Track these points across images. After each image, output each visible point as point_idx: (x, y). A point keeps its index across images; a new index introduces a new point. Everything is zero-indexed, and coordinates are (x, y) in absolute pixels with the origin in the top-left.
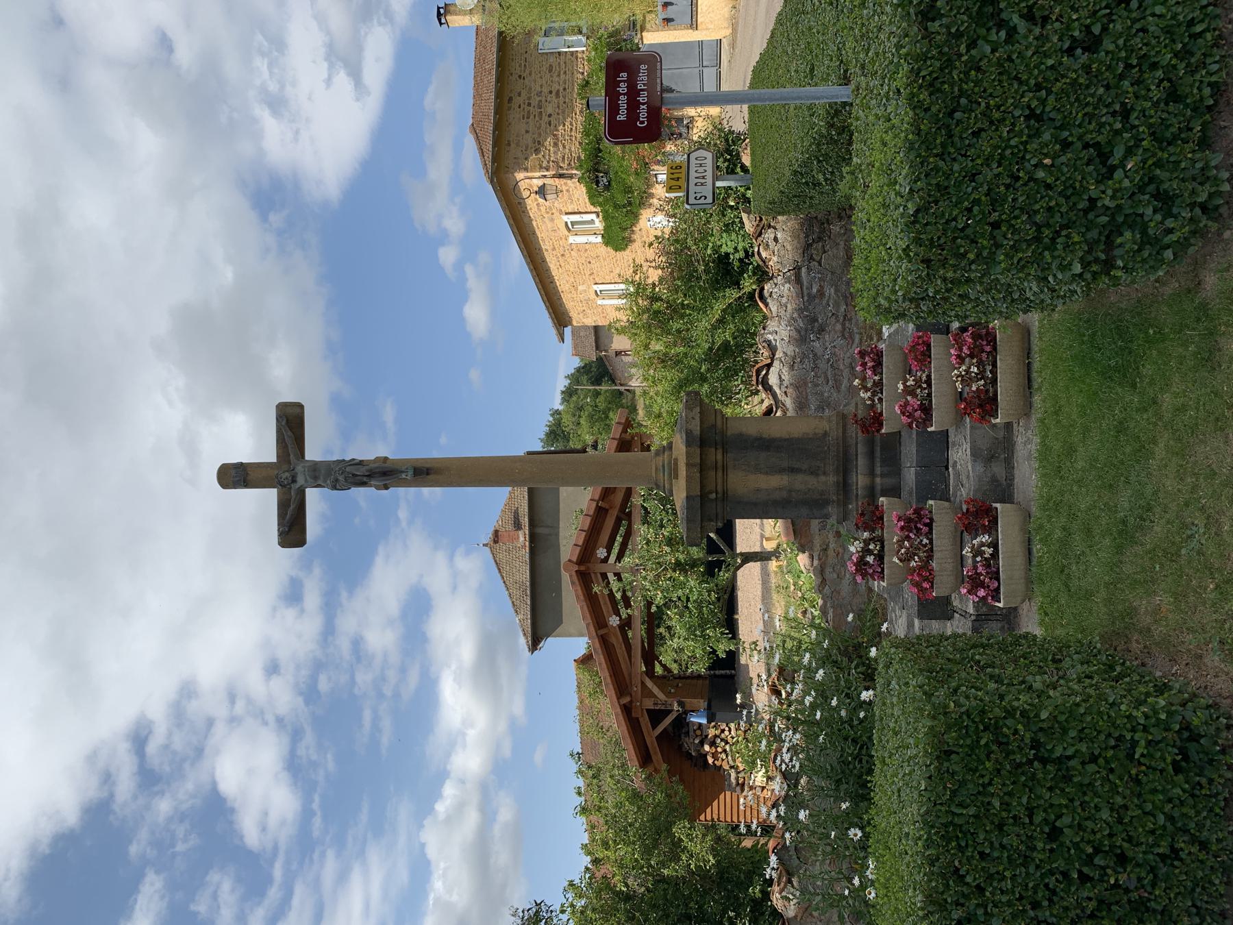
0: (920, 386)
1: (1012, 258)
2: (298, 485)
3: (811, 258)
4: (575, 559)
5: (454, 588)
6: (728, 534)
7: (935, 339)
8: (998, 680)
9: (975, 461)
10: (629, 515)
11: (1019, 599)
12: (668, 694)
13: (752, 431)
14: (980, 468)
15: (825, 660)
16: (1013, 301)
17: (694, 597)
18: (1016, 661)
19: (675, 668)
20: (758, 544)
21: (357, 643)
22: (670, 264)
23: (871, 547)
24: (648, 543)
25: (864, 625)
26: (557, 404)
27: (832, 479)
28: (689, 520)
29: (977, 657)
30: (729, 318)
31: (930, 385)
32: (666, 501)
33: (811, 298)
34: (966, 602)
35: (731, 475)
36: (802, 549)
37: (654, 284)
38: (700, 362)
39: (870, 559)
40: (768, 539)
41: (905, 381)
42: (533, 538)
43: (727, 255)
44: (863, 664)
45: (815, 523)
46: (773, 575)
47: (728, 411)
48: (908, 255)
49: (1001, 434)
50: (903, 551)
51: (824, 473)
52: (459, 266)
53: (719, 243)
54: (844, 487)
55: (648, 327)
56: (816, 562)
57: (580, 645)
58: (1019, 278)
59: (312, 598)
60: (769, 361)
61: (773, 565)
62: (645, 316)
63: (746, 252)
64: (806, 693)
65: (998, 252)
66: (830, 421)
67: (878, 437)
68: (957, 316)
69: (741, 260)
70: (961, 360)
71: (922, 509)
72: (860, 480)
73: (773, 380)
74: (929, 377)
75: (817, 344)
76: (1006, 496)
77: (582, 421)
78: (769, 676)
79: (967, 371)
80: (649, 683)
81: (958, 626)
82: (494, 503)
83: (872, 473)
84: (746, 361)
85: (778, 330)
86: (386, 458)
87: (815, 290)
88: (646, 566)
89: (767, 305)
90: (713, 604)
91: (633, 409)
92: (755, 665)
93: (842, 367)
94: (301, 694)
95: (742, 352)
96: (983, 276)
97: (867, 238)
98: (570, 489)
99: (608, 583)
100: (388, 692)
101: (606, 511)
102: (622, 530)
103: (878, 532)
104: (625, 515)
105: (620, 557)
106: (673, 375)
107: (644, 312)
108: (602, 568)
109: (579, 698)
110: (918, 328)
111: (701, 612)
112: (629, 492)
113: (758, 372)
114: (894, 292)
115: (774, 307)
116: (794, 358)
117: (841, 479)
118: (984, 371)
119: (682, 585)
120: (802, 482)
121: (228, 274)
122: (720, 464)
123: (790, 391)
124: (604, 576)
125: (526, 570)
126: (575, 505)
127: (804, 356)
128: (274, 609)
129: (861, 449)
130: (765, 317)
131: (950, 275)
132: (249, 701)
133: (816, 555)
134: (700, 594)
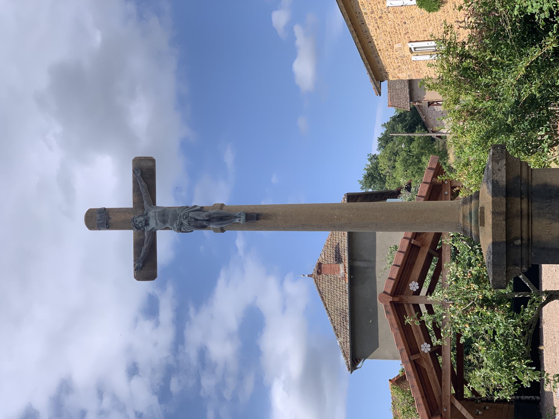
2: (149, 228)
4: (389, 291)
5: (284, 309)
6: (535, 276)
10: (440, 252)
21: (203, 353)
22: (479, 24)
24: (457, 280)
26: (375, 150)
28: (495, 265)
30: (535, 74)
32: (474, 242)
38: (505, 115)
42: (352, 270)
43: (533, 15)
47: (532, 161)
52: (289, 27)
55: (458, 85)
57: (395, 367)
59: (166, 313)
62: (455, 73)
69: (545, 20)
77: (397, 165)
80: (458, 405)
82: (317, 244)
86: (222, 205)
88: (455, 299)
90: (519, 338)
91: (444, 154)
94: (155, 393)
95: (548, 105)
98: (381, 233)
99: (420, 314)
100: (227, 395)
101: (419, 248)
102: (433, 265)
104: (436, 251)
105: (430, 291)
106: (483, 126)
107: (454, 69)
111: (507, 345)
112: (438, 236)
119: (490, 320)
121: (98, 38)
122: (525, 212)
124: (417, 307)
125: (347, 298)
126: (388, 249)
128: (136, 320)
132: (115, 398)
134: (506, 328)
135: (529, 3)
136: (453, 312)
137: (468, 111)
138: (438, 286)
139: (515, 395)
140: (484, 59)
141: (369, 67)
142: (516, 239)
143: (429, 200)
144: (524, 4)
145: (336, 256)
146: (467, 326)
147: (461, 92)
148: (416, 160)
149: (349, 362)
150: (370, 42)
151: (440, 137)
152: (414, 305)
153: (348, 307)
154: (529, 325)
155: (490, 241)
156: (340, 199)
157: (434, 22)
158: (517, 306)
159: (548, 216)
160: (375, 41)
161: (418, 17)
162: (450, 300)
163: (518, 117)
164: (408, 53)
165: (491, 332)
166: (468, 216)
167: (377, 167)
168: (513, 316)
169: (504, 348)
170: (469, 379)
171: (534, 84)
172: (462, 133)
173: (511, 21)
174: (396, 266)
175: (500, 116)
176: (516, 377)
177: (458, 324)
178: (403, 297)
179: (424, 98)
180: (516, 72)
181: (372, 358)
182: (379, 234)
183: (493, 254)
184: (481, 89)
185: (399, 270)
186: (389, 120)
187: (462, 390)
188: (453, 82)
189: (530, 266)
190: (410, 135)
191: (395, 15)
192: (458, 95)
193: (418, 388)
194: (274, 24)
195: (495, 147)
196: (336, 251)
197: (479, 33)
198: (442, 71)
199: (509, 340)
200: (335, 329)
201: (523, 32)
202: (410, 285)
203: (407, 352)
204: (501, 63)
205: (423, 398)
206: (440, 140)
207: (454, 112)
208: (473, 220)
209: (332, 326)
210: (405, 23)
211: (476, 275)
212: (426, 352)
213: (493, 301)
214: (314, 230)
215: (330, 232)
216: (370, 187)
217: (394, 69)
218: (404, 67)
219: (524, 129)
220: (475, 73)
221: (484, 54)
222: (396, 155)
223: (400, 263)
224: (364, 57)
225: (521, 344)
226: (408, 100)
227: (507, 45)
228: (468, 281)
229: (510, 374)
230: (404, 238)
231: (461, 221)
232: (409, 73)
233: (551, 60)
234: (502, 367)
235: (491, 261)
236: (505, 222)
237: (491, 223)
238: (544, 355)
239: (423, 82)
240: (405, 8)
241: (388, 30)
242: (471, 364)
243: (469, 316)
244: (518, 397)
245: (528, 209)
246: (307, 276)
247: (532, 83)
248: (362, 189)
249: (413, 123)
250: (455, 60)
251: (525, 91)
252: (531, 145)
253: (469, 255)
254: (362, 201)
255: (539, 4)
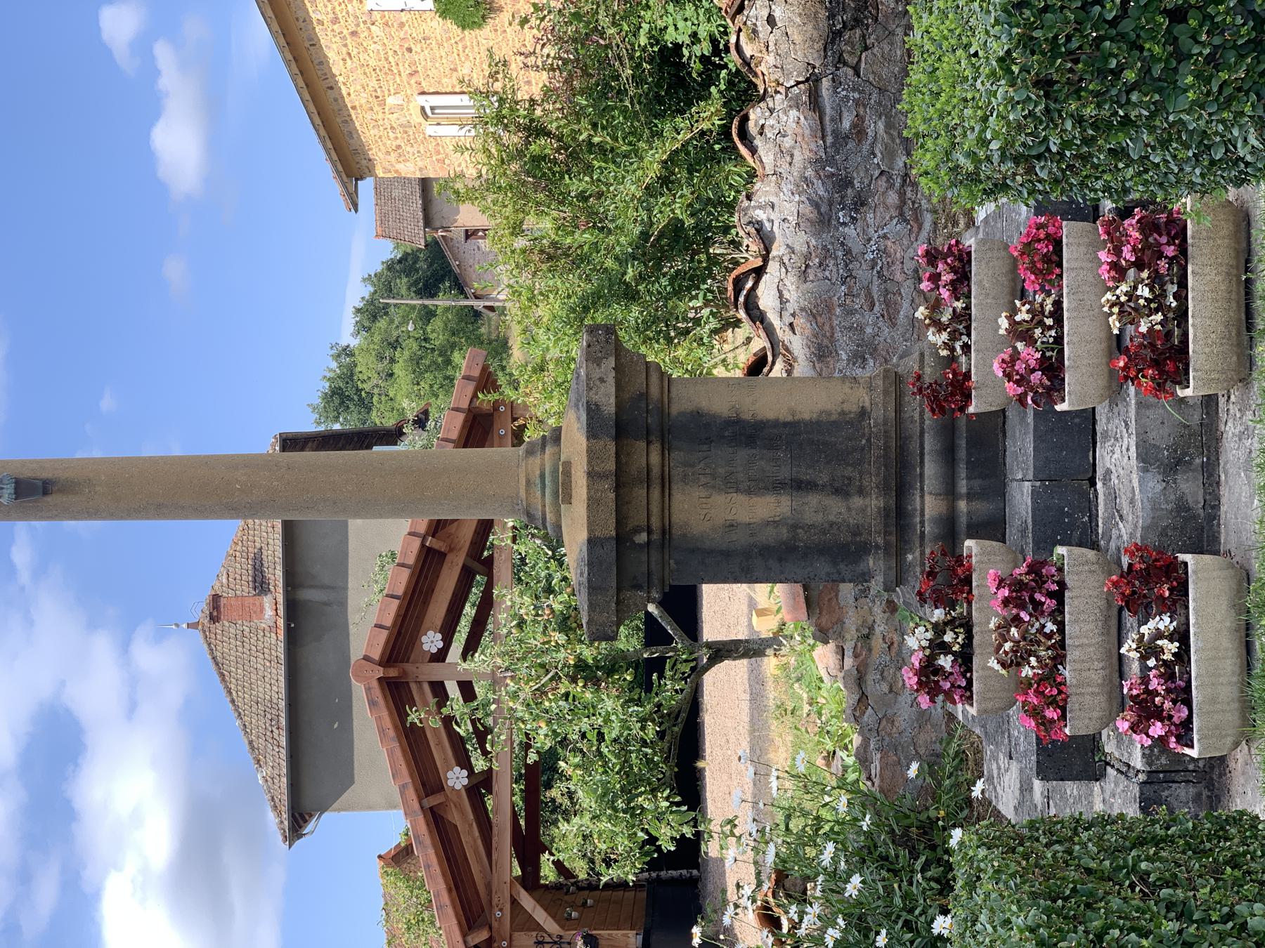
0: (1041, 323)
1: (1208, 81)
3: (841, 61)
4: (376, 654)
5: (132, 708)
7: (1070, 231)
8: (1183, 914)
9: (1145, 470)
10: (489, 562)
11: (1229, 741)
12: (565, 922)
13: (720, 406)
14: (1155, 484)
15: (867, 855)
16: (1213, 162)
17: (612, 733)
18: (1216, 872)
19: (581, 870)
20: (744, 621)
23: (948, 637)
24: (521, 624)
25: (939, 785)
26: (348, 336)
27: (874, 503)
28: (594, 588)
29: (1143, 865)
30: (681, 174)
31: (1059, 321)
32: (554, 542)
33: (841, 139)
34: (1129, 748)
35: (678, 497)
36: (823, 635)
37: (532, 100)
39: (946, 662)
40: (762, 613)
41: (1014, 311)
42: (293, 609)
43: (678, 47)
44: (939, 861)
45: (847, 590)
46: (770, 685)
48: (1009, 71)
49: (1196, 418)
50: (1008, 646)
51: (861, 492)
52: (142, 46)
53: (660, 24)
54: (899, 518)
55: (519, 192)
56: (849, 662)
58: (1223, 121)
60: (759, 262)
61: (770, 664)
62: (515, 166)
63: (714, 41)
64: (827, 921)
65: (1183, 68)
66: (871, 388)
67: (962, 422)
68: (1107, 189)
70: (1119, 271)
71: (1044, 563)
72: (928, 506)
73: (767, 299)
74: (1058, 304)
75: (850, 231)
76: (1204, 537)
77: (398, 369)
78: (759, 884)
79: (1131, 296)
80: (527, 901)
81: (1114, 797)
82: (214, 549)
83: (950, 492)
84: (713, 260)
85: (776, 200)
87: (846, 124)
88: (521, 672)
89: (753, 151)
91: (501, 347)
92: (737, 867)
93: (899, 277)
95: (708, 242)
96: (1152, 116)
97: (934, 31)
98: (359, 521)
101: (442, 555)
102: (476, 593)
103: (961, 609)
104: (480, 562)
105: (471, 647)
107: (512, 158)
108: (435, 672)
109: (389, 932)
110: (1039, 210)
112: (486, 527)
113: (738, 284)
114: (984, 143)
115: (767, 154)
116: (808, 257)
117: (892, 503)
118: (1164, 294)
120: (821, 510)
122: (656, 471)
123: (800, 322)
124: (439, 689)
125: (279, 675)
126: (374, 560)
127: (826, 253)
129: (930, 443)
130: (752, 175)
131: (1089, 111)
133: (849, 647)
134: (625, 725)
135: (670, 20)
136: (514, 696)
137: (542, 252)
138: (486, 639)
139: (642, 870)
140: (574, 139)
141: (330, 145)
142: (637, 530)
143: (465, 446)
144: (659, 22)
145: (254, 577)
146: (543, 725)
147: (527, 209)
148: (440, 360)
149: (286, 823)
150: (331, 88)
151: (491, 309)
152: (432, 684)
153: (282, 695)
154: (674, 716)
155: (583, 536)
156: (266, 445)
157: (464, 54)
158: (647, 673)
159: (703, 479)
160: (343, 87)
161: (439, 38)
162: (507, 669)
163: (646, 266)
164: (417, 118)
165: (592, 736)
166: (538, 481)
167: (352, 375)
168: (639, 699)
169: (620, 770)
170: (552, 841)
171: (681, 197)
172: (529, 300)
173: (631, 58)
174: (392, 596)
175: (609, 263)
176: (647, 832)
177: (523, 722)
178: (409, 667)
179: (456, 221)
180: (640, 173)
181: (339, 810)
182: (355, 525)
183: (590, 564)
184: (570, 204)
185: (400, 607)
186: (380, 268)
187: (537, 867)
188: (511, 186)
189: (667, 590)
190: (427, 302)
191: (387, 29)
192: (521, 216)
193: (438, 870)
194: (105, 36)
195: (592, 330)
196: (254, 566)
197: (566, 82)
198: (485, 160)
199: (631, 752)
200: (253, 748)
201: (658, 85)
202: (424, 639)
203: (416, 790)
204: (612, 150)
205: (450, 890)
206: (491, 314)
207: (513, 252)
208: (548, 491)
209: (246, 742)
210: (410, 50)
211: (562, 612)
212: (458, 787)
213: (598, 668)
214: (186, 518)
215: (240, 523)
216: (336, 419)
217: (388, 153)
218: (408, 149)
219: (659, 293)
220: (557, 169)
221: (576, 127)
222: (395, 348)
223: (400, 591)
224: (318, 121)
225: (656, 759)
226: (421, 224)
227: (624, 111)
228: (546, 627)
229: (633, 826)
230: (410, 534)
231: (523, 493)
232: (420, 164)
233: (717, 147)
234: (615, 810)
235: (584, 579)
236: (612, 496)
237: (585, 496)
238: (707, 780)
239: (447, 183)
240: (408, 16)
241: (372, 63)
242: (556, 808)
243: (547, 704)
244: (654, 875)
245: (663, 466)
246: (185, 626)
247: (674, 195)
248: (319, 424)
249: (432, 275)
250: (514, 139)
251: (661, 212)
252: (675, 328)
253: (548, 568)
254: (317, 449)
255: (689, 23)
